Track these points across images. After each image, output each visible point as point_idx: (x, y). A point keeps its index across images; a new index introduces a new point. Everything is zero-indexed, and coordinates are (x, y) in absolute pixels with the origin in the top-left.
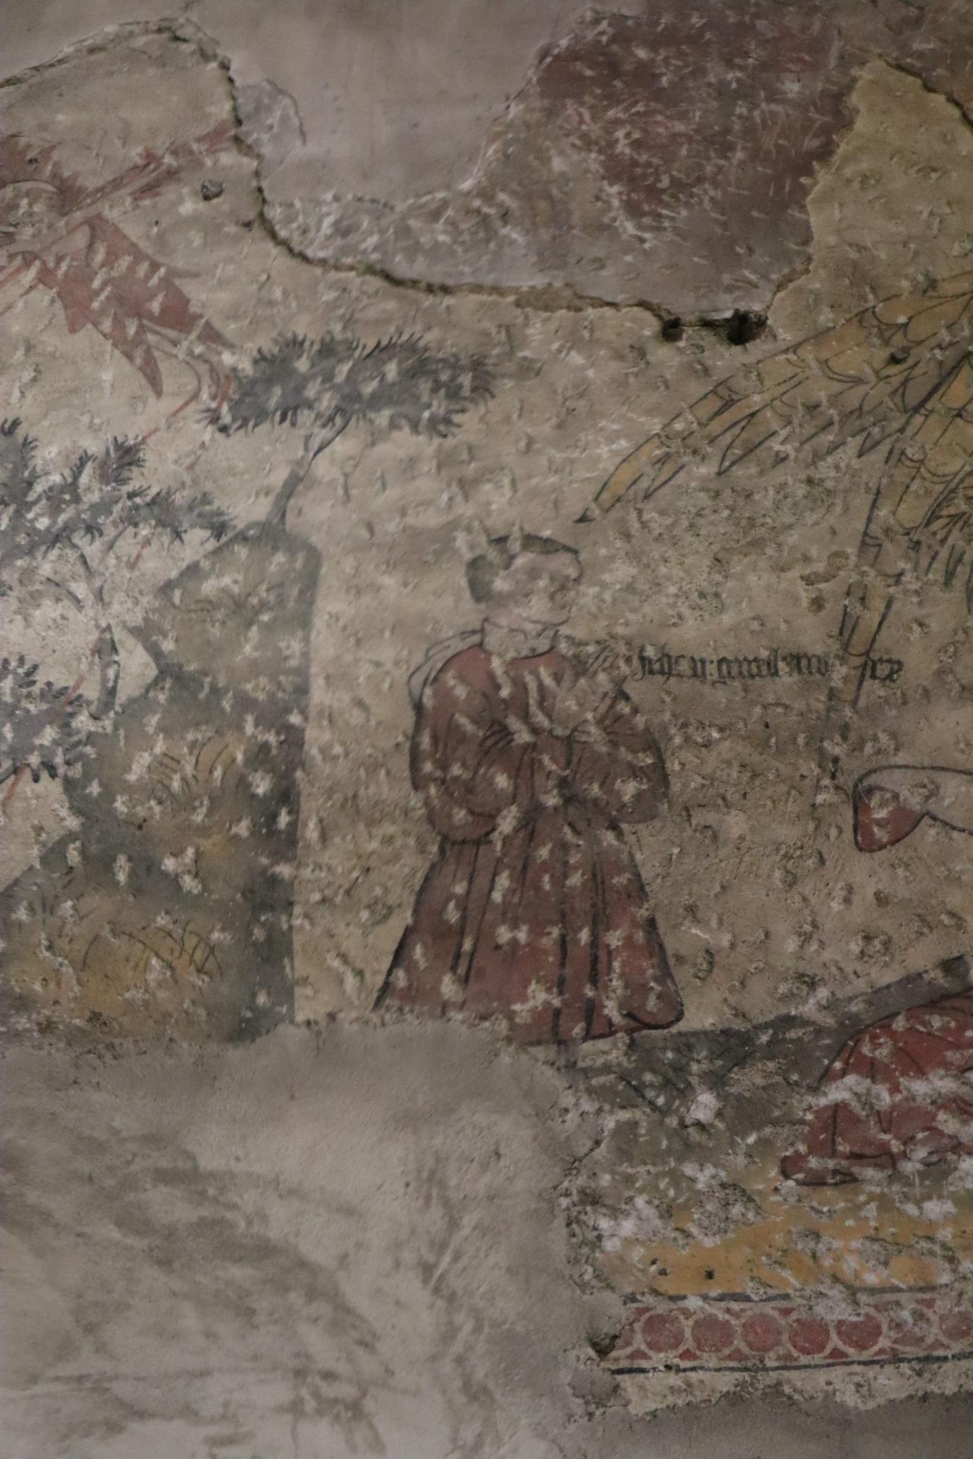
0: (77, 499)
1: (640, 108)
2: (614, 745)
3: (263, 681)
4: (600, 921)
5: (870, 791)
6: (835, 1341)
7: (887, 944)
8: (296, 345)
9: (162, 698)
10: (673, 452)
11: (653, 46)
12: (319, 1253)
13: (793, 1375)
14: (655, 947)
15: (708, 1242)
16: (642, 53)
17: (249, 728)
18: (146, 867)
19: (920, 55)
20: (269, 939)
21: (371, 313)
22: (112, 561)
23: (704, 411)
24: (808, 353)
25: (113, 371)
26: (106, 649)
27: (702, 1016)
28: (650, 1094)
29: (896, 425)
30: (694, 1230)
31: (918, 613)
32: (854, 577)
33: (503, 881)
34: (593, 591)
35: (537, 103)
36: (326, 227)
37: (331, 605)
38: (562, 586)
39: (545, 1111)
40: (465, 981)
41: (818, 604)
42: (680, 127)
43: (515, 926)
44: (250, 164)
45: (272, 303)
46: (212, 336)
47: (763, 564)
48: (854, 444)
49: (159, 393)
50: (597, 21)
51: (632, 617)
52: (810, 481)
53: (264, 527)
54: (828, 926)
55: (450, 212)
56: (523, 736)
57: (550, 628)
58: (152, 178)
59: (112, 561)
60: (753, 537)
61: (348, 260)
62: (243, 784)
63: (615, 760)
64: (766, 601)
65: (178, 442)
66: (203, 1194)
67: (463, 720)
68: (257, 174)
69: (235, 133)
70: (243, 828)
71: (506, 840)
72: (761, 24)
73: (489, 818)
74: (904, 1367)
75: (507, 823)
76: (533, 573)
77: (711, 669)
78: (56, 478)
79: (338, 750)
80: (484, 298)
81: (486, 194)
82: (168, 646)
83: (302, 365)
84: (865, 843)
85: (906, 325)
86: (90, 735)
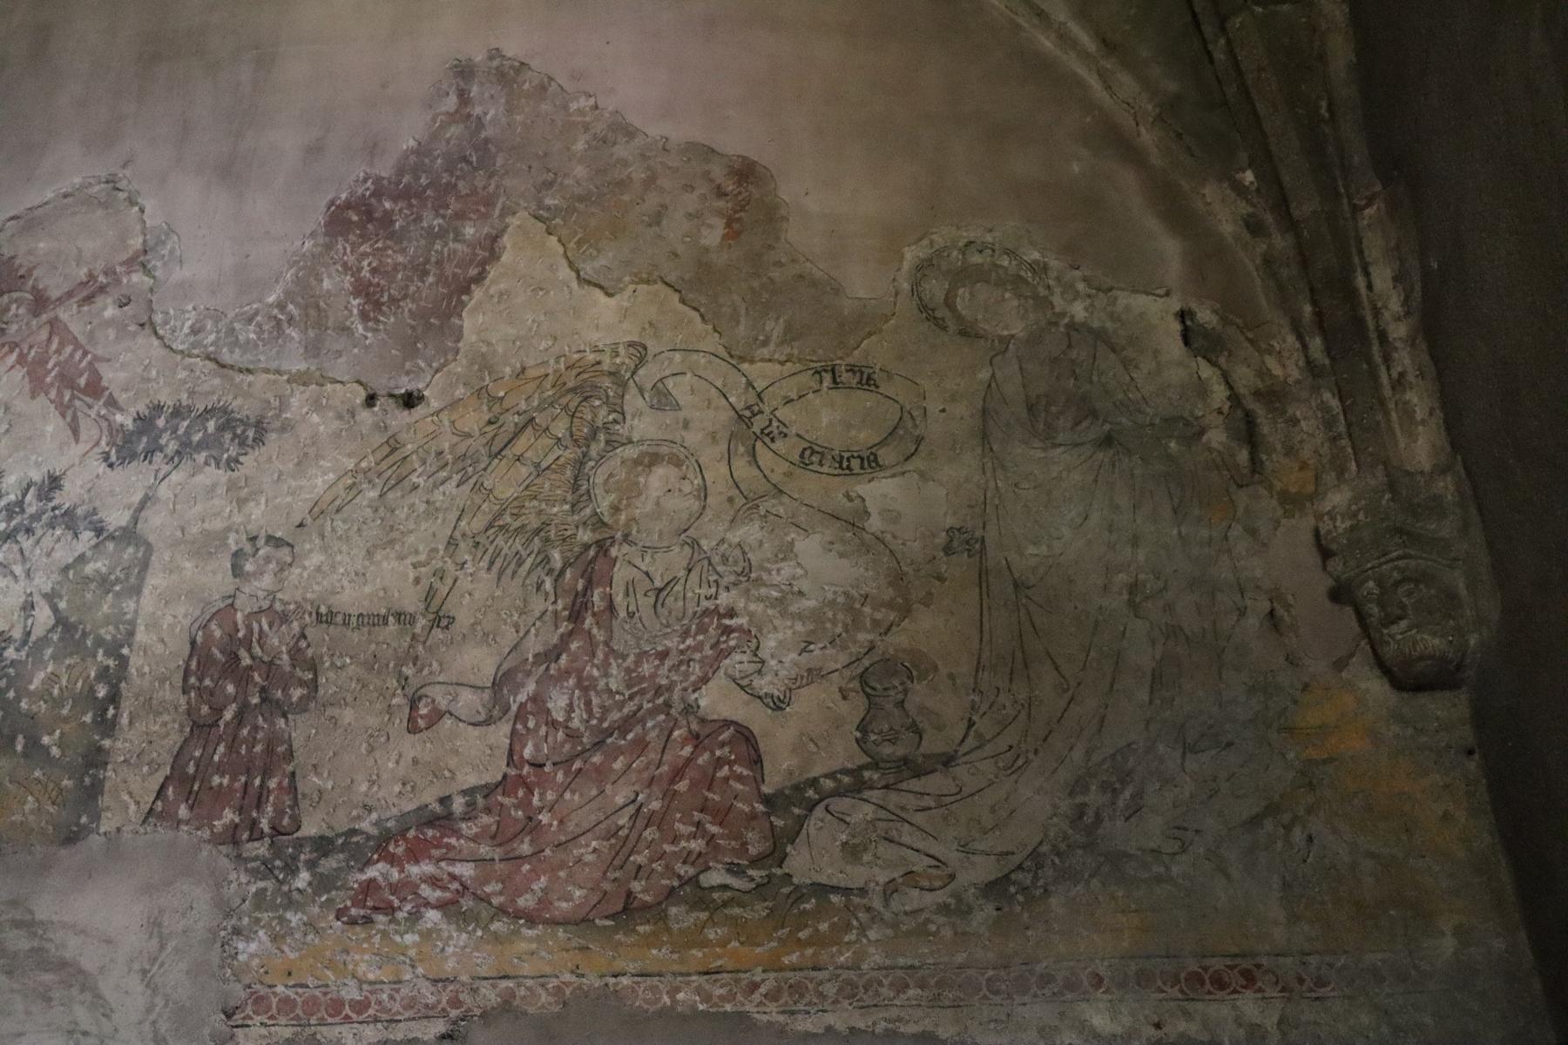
0: (23, 511)
1: (380, 245)
2: (294, 666)
3: (111, 628)
4: (267, 774)
5: (420, 698)
6: (347, 1010)
7: (413, 788)
8: (158, 408)
9: (55, 637)
10: (356, 480)
11: (395, 199)
12: (88, 963)
13: (323, 1029)
14: (293, 789)
15: (292, 956)
16: (387, 205)
17: (100, 657)
18: (33, 744)
19: (548, 209)
20: (93, 785)
21: (206, 387)
22: (38, 551)
23: (379, 455)
24: (444, 416)
25: (53, 426)
26: (29, 607)
27: (310, 829)
28: (276, 872)
29: (483, 466)
30: (286, 949)
31: (470, 586)
32: (440, 564)
33: (221, 749)
34: (298, 571)
35: (321, 240)
36: (186, 330)
37: (156, 580)
38: (283, 567)
39: (219, 882)
40: (191, 808)
41: (417, 581)
42: (400, 259)
43: (222, 776)
44: (148, 281)
45: (149, 380)
46: (112, 403)
47: (392, 555)
48: (456, 478)
49: (77, 441)
50: (365, 180)
51: (316, 588)
52: (428, 502)
53: (124, 529)
54: (385, 776)
55: (259, 318)
56: (246, 661)
57: (271, 595)
58: (90, 291)
59: (38, 551)
60: (390, 538)
61: (196, 352)
62: (92, 690)
63: (292, 675)
64: (391, 579)
65: (87, 476)
66: (35, 934)
67: (215, 651)
68: (151, 290)
69: (139, 261)
70: (88, 718)
71: (227, 724)
72: (461, 184)
73: (218, 711)
74: (379, 1025)
75: (228, 715)
76: (268, 560)
77: (354, 620)
78: (12, 497)
79: (146, 669)
80: (271, 377)
81: (281, 306)
82: (62, 605)
83: (161, 422)
84: (412, 729)
85: (502, 398)
86: (12, 661)
